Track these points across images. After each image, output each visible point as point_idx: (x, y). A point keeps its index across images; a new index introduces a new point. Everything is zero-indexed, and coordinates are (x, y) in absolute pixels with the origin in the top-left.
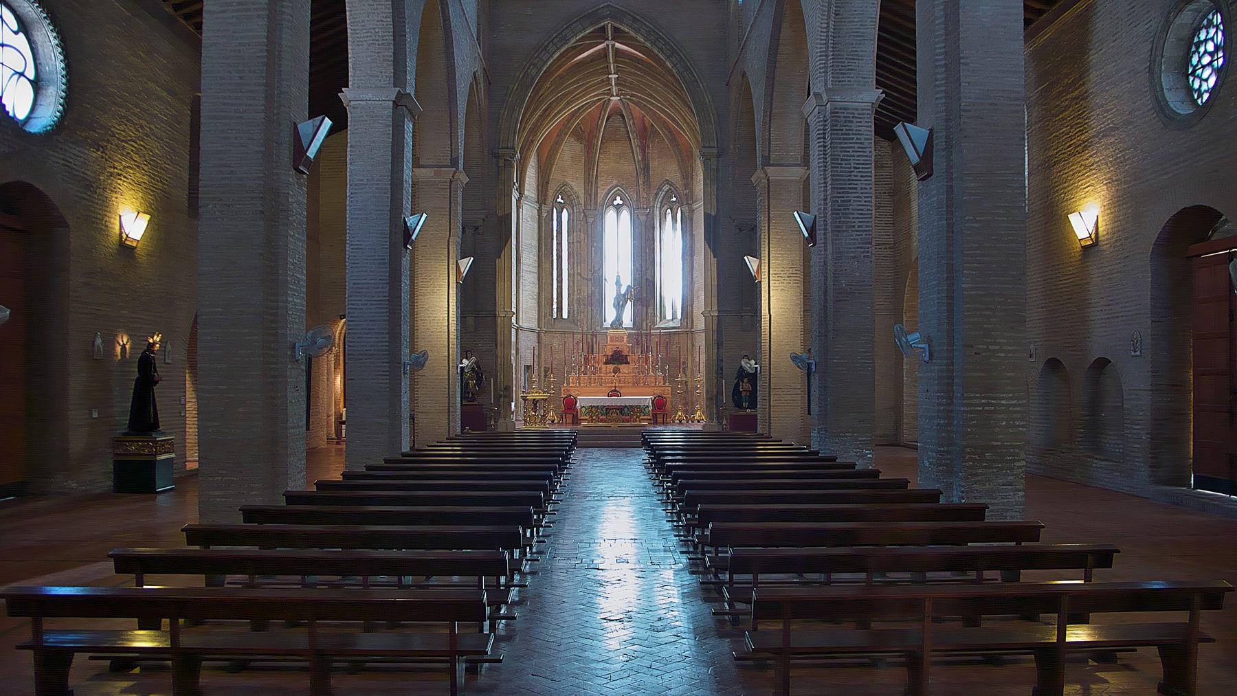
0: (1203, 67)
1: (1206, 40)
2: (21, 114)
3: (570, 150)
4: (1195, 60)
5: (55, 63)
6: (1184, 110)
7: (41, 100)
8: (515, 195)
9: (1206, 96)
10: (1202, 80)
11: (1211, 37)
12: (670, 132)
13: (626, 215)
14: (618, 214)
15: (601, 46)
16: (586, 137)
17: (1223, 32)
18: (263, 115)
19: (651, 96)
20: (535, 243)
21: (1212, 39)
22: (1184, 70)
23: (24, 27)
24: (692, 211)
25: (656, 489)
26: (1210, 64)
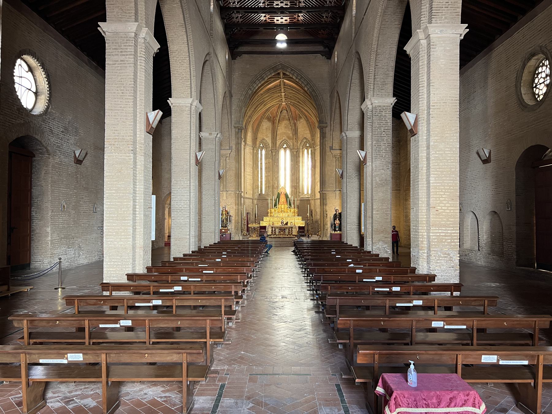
0: (540, 84)
1: (541, 72)
2: (30, 107)
3: (266, 125)
4: (536, 81)
5: (44, 85)
6: (531, 103)
7: (38, 100)
8: (243, 143)
9: (541, 97)
10: (539, 89)
11: (544, 71)
12: (306, 117)
13: (288, 151)
14: (285, 152)
15: (278, 81)
16: (273, 120)
17: (550, 69)
18: (132, 109)
19: (298, 102)
20: (251, 163)
21: (544, 72)
22: (532, 86)
23: (31, 69)
24: (315, 150)
25: (300, 266)
26: (544, 82)
